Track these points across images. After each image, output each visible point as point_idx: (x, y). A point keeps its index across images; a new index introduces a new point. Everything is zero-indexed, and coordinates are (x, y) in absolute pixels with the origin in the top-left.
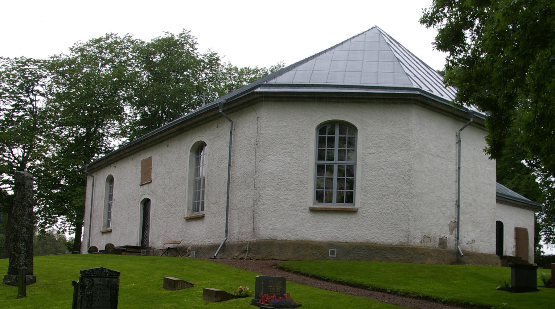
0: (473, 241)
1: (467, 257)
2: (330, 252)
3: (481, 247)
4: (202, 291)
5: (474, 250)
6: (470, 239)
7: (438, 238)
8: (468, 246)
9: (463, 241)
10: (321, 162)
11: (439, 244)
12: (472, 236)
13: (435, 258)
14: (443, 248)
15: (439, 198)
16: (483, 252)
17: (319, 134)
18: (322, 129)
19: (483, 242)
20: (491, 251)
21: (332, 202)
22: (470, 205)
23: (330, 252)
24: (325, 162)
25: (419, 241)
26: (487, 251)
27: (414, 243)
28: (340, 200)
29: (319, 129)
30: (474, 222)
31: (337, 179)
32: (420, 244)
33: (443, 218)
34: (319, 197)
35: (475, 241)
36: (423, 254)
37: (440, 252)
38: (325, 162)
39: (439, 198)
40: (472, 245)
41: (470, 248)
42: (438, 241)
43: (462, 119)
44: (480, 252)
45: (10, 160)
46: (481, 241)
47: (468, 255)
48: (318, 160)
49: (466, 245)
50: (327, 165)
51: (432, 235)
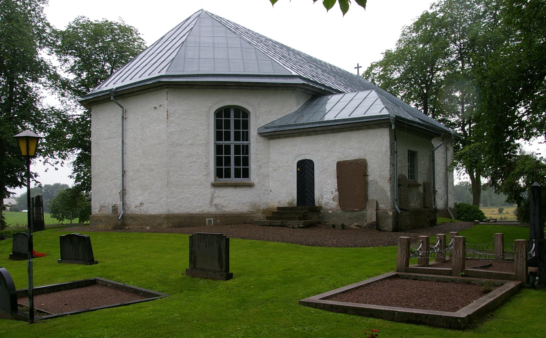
0: (141, 204)
1: (132, 220)
2: (207, 221)
3: (150, 209)
4: (9, 255)
5: (142, 213)
6: (138, 203)
7: (111, 206)
8: (137, 209)
9: (132, 206)
10: (220, 142)
11: (112, 211)
12: (141, 199)
13: (104, 223)
14: (115, 214)
15: (111, 173)
16: (152, 214)
17: (217, 118)
18: (218, 113)
19: (152, 203)
20: (162, 212)
21: (230, 178)
22: (138, 171)
23: (207, 221)
24: (223, 143)
25: (97, 210)
26: (157, 212)
27: (95, 212)
28: (237, 175)
29: (216, 114)
30: (142, 186)
31: (231, 154)
32: (99, 213)
33: (115, 188)
34: (219, 173)
35: (143, 204)
36: (97, 220)
37: (108, 217)
38: (223, 143)
39: (111, 173)
40: (141, 208)
41: (139, 211)
42: (111, 208)
43: (126, 96)
44: (149, 214)
45: (471, 155)
46: (149, 203)
47: (135, 218)
48: (217, 141)
49: (134, 208)
50: (224, 145)
51: (107, 204)
